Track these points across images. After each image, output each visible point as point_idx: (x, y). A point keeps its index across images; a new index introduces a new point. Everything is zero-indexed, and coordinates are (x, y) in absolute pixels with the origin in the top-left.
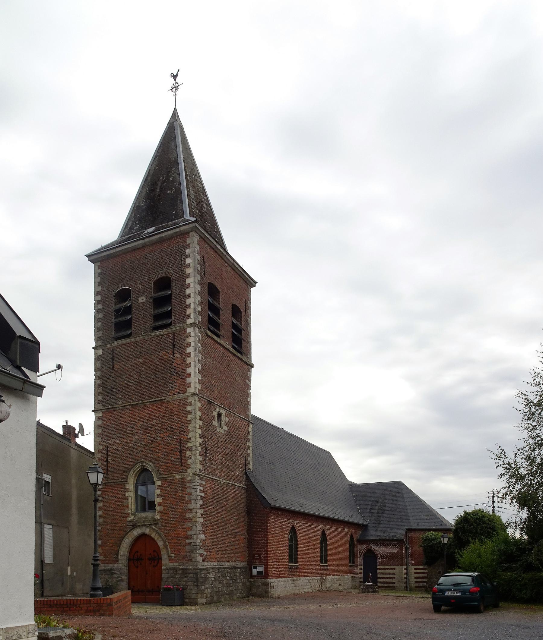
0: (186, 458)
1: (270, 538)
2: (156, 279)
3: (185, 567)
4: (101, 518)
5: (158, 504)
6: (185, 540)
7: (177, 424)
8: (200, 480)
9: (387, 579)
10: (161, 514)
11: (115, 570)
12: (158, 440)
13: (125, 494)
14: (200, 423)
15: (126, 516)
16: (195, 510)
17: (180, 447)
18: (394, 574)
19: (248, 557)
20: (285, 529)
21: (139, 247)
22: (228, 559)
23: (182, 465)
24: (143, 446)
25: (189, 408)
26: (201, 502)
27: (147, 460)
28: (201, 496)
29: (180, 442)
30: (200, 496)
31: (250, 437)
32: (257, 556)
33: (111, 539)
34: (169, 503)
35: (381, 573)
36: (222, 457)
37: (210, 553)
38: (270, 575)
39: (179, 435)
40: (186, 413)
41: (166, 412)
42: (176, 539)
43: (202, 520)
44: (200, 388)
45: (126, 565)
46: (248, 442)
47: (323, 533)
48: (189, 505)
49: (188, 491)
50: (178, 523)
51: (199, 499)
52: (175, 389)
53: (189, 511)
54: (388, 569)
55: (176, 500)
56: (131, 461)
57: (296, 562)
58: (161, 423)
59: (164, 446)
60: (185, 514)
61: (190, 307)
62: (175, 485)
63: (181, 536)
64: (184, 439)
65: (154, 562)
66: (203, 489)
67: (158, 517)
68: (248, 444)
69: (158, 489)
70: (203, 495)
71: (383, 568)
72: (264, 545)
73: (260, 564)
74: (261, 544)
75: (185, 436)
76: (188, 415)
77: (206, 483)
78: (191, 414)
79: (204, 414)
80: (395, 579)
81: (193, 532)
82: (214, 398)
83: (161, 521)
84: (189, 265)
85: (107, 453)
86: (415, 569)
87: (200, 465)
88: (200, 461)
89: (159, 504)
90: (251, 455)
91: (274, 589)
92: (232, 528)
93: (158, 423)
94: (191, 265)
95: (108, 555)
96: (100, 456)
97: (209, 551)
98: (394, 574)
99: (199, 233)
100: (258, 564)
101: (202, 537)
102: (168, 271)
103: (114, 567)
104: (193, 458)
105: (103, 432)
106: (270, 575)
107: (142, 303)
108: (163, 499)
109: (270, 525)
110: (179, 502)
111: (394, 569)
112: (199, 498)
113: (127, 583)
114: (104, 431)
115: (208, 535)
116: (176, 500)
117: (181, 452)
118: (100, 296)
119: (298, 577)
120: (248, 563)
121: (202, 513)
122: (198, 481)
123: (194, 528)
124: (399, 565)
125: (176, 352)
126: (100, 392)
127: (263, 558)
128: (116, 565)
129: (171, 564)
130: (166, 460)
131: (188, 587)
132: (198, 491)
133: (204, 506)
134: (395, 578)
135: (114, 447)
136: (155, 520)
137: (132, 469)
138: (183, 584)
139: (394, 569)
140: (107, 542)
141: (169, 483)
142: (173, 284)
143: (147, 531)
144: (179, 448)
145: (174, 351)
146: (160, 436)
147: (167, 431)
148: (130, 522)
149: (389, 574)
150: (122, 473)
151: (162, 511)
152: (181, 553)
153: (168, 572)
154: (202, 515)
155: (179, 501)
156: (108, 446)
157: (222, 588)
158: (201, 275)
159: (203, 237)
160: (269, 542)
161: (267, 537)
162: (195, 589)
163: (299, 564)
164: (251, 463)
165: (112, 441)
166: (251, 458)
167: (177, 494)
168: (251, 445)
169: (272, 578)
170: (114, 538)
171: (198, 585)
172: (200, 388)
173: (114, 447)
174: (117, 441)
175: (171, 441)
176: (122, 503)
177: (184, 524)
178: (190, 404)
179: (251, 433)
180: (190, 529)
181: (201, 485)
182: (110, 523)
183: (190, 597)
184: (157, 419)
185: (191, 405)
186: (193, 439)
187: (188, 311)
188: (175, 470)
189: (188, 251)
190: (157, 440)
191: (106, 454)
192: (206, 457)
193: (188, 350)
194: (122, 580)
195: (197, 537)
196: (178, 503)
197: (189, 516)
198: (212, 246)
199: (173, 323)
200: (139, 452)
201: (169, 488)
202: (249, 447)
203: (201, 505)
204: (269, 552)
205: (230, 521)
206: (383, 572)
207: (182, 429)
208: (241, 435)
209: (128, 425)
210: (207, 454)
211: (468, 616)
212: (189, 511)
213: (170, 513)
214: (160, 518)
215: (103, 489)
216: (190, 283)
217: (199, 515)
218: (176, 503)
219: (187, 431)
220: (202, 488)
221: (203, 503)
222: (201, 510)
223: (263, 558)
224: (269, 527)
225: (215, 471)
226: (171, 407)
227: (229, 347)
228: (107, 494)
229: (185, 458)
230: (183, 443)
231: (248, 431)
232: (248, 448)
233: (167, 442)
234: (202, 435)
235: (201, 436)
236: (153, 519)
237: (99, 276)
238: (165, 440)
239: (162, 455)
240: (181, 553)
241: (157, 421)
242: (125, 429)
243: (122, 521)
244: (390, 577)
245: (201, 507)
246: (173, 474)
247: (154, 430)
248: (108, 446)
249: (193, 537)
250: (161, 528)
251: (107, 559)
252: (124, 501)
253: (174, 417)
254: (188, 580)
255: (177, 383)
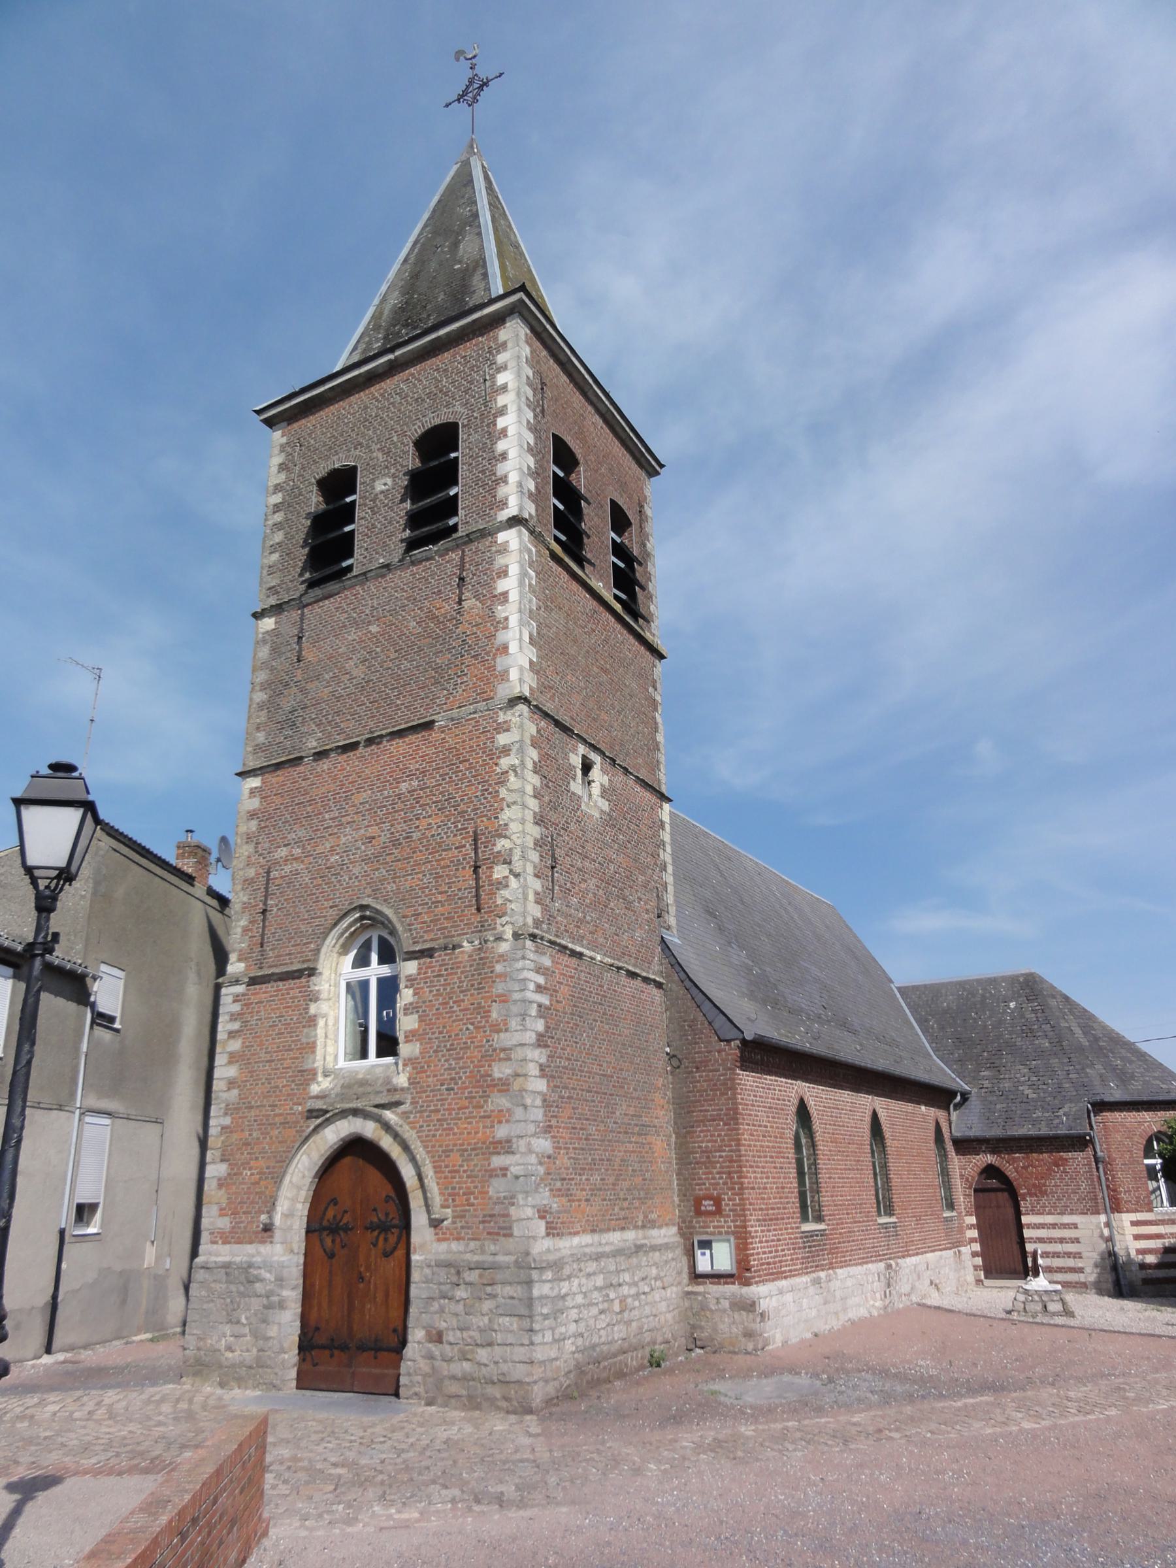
0: (492, 885)
1: (745, 1140)
2: (420, 433)
3: (490, 1259)
4: (234, 1088)
5: (406, 1037)
6: (488, 1159)
7: (466, 786)
8: (537, 952)
9: (1058, 1257)
10: (414, 1068)
11: (260, 1268)
12: (411, 837)
13: (308, 1009)
14: (535, 780)
15: (305, 1080)
16: (518, 1054)
17: (476, 853)
18: (1077, 1241)
19: (679, 1206)
20: (782, 1110)
21: (380, 371)
22: (624, 1218)
23: (479, 910)
24: (366, 860)
25: (503, 739)
26: (540, 1026)
27: (377, 898)
28: (540, 1006)
29: (475, 840)
30: (535, 1005)
31: (667, 837)
32: (708, 1205)
33: (257, 1158)
34: (440, 1033)
35: (1037, 1238)
36: (597, 886)
37: (569, 1201)
38: (755, 1272)
39: (472, 819)
40: (495, 754)
41: (438, 756)
42: (459, 1154)
43: (541, 1085)
44: (534, 685)
45: (295, 1247)
46: (661, 852)
47: (875, 1116)
48: (502, 1035)
49: (500, 988)
50: (466, 1098)
51: (534, 1012)
52: (464, 691)
53: (502, 1055)
54: (1054, 1226)
55: (462, 1020)
56: (331, 907)
57: (819, 1219)
58: (421, 790)
59: (430, 854)
60: (490, 1066)
61: (506, 482)
62: (459, 971)
63: (475, 1144)
64: (486, 828)
65: (386, 1240)
66: (546, 983)
67: (402, 1080)
68: (662, 856)
69: (406, 987)
70: (545, 1000)
71: (1040, 1224)
72: (728, 1167)
73: (720, 1233)
74: (718, 1162)
75: (489, 819)
76: (499, 758)
77: (553, 962)
78: (509, 755)
79: (544, 756)
80: (1081, 1258)
81: (516, 1129)
82: (573, 719)
83: (412, 1094)
84: (504, 388)
85: (267, 888)
86: (1135, 1224)
87: (536, 905)
88: (537, 893)
89: (411, 1036)
90: (670, 888)
91: (770, 1323)
92: (631, 1111)
93: (414, 791)
94: (510, 386)
95: (244, 1213)
96: (245, 899)
97: (567, 1195)
98: (1077, 1241)
99: (531, 320)
100: (713, 1234)
101: (544, 1144)
102: (451, 410)
103: (259, 1253)
104: (513, 882)
105: (261, 829)
106: (755, 1272)
107: (382, 492)
108: (421, 1020)
109: (742, 1099)
110: (471, 1027)
111: (1075, 1226)
112: (533, 1011)
113: (295, 1314)
114: (263, 824)
115: (561, 1137)
116: (462, 1020)
117: (476, 868)
118: (280, 495)
119: (829, 1269)
120: (680, 1228)
121: (543, 1060)
122: (531, 956)
123: (519, 1113)
124: (1086, 1214)
125: (467, 594)
126: (259, 724)
127: (730, 1210)
128: (265, 1249)
129: (444, 1246)
130: (434, 894)
131: (499, 1337)
132: (532, 986)
133: (549, 1037)
134: (1080, 1253)
135: (288, 868)
136: (394, 1090)
137: (331, 930)
138: (481, 1324)
139: (1075, 1226)
140: (245, 1169)
141: (441, 965)
142: (462, 436)
143: (369, 1129)
144: (473, 855)
145: (461, 593)
146: (418, 827)
147: (439, 810)
148: (317, 1097)
149: (1062, 1241)
150: (305, 944)
151: (418, 1058)
152: (473, 1205)
153: (430, 1277)
154: (542, 1068)
155: (472, 1024)
156: (269, 868)
157: (609, 1328)
158: (534, 410)
159: (539, 329)
160: (745, 1156)
161: (739, 1140)
162: (522, 1345)
163: (828, 1225)
164: (672, 910)
165: (283, 852)
166: (670, 898)
167: (463, 1001)
168: (668, 859)
169: (760, 1282)
170: (267, 1152)
171: (531, 1330)
172: (534, 685)
173: (288, 868)
174: (297, 851)
175: (448, 837)
176: (297, 1036)
177: (486, 1102)
178: (505, 728)
179: (667, 827)
180: (502, 1116)
181: (539, 970)
182: (259, 1103)
183: (504, 1374)
184: (412, 780)
185: (508, 730)
186: (514, 827)
187: (502, 491)
188: (460, 926)
189: (501, 358)
190: (408, 837)
191: (263, 890)
192: (553, 882)
193: (502, 585)
194: (282, 1305)
195: (529, 1144)
196: (467, 1029)
197: (500, 1071)
198: (562, 357)
199: (460, 526)
200: (357, 877)
201: (440, 981)
202: (665, 866)
203: (540, 1036)
204: (747, 1188)
205: (623, 1087)
206: (1039, 1236)
207: (483, 801)
208: (644, 829)
209: (331, 803)
210: (556, 875)
211: (347, 1079)
212: (502, 1055)
213: (440, 1064)
214: (410, 1084)
215: (247, 995)
216: (507, 427)
217: (533, 1070)
218: (461, 1030)
219: (496, 805)
220: (541, 980)
221: (547, 1027)
222: (541, 1052)
223: (730, 1210)
224: (741, 1104)
225: (579, 927)
226: (451, 742)
227: (608, 596)
228: (258, 1012)
229: (489, 885)
230: (483, 840)
231: (661, 821)
232: (664, 868)
233: (436, 843)
234: (541, 816)
235: (539, 821)
236: (388, 1087)
237: (282, 451)
238: (433, 836)
239: (422, 880)
240: (473, 1205)
241: (410, 784)
242: (320, 814)
243: (295, 1094)
244: (1065, 1253)
245: (541, 1041)
246: (453, 936)
247: (402, 810)
248: (269, 868)
249: (514, 1146)
250: (412, 1116)
251: (239, 1228)
252: (305, 1030)
253: (458, 767)
254: (497, 1307)
255: (469, 676)
